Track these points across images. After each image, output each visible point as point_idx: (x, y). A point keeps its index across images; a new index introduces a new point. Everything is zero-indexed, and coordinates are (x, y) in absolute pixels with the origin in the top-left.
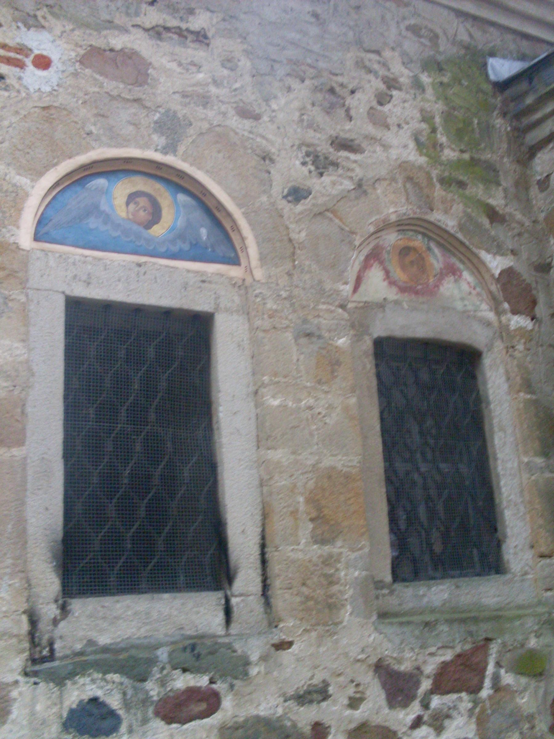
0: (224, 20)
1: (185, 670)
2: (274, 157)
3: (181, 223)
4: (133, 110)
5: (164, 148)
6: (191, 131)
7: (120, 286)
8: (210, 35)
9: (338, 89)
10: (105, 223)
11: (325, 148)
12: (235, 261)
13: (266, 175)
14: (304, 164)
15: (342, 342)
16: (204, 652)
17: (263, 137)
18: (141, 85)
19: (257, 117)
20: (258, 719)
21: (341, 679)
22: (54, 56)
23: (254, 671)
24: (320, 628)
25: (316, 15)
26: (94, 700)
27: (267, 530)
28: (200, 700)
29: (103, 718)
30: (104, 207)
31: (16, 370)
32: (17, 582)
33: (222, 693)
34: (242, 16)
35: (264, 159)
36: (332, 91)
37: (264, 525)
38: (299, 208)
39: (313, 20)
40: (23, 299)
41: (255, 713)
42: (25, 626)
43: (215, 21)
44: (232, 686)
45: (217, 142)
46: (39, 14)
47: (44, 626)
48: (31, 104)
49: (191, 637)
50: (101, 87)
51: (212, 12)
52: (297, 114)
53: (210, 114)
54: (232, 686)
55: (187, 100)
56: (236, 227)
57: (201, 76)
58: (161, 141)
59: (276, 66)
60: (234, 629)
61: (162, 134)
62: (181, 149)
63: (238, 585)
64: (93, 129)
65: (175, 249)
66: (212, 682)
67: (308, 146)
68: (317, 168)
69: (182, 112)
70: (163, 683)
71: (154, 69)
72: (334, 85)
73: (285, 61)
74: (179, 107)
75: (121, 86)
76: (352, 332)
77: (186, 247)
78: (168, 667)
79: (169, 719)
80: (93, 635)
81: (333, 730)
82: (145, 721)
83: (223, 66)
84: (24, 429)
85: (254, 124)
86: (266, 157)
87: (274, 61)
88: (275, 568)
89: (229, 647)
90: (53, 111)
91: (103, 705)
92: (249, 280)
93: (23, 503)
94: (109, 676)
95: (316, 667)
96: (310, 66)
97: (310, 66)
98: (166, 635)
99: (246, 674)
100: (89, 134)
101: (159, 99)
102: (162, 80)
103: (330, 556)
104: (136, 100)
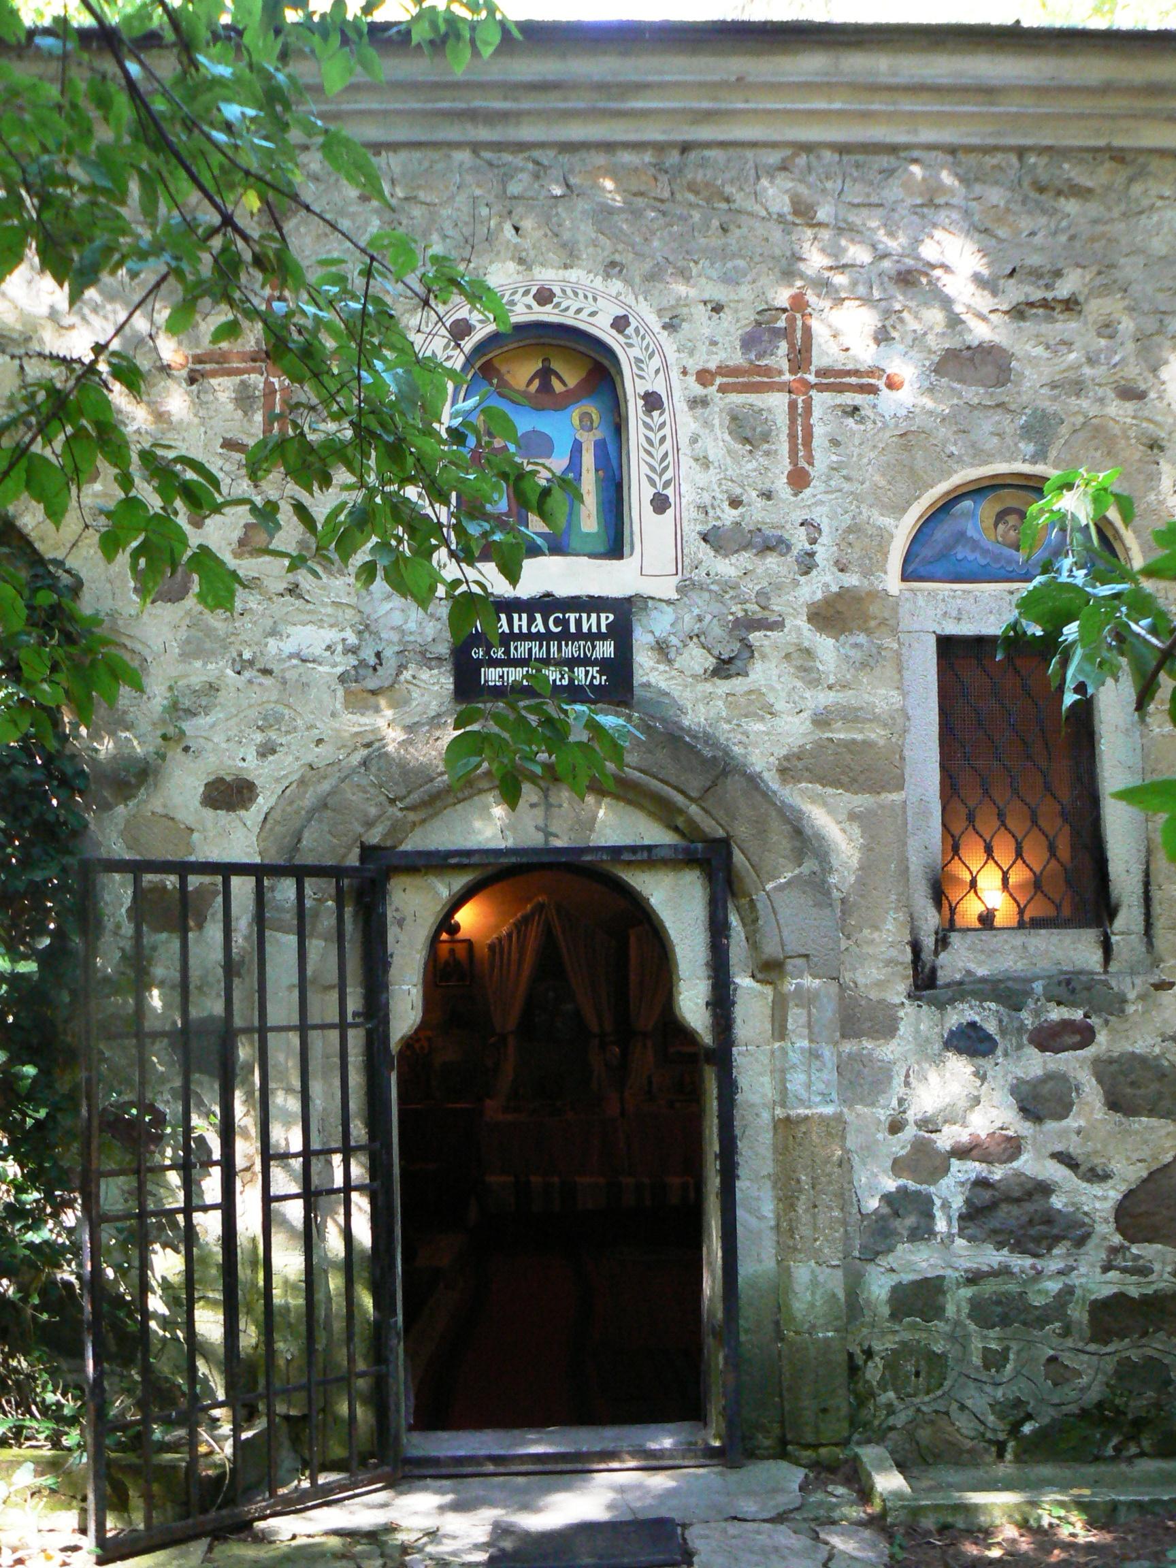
0: (1099, 273)
1: (1059, 1003)
2: (1164, 443)
5: (1033, 457)
6: (1064, 430)
7: (992, 618)
8: (1081, 299)
10: (973, 550)
16: (1078, 987)
17: (1150, 420)
19: (1141, 396)
23: (1131, 1009)
26: (973, 1025)
27: (1152, 867)
28: (1074, 1033)
29: (981, 1041)
31: (893, 718)
32: (901, 916)
33: (1097, 1028)
34: (1122, 261)
35: (1151, 447)
37: (1148, 863)
40: (896, 646)
42: (908, 956)
43: (1088, 278)
44: (1107, 1022)
45: (1094, 437)
47: (927, 956)
48: (888, 434)
49: (1066, 973)
50: (960, 397)
51: (1084, 267)
53: (1085, 404)
54: (1107, 1022)
55: (1056, 392)
57: (1073, 356)
58: (1028, 448)
60: (1113, 968)
61: (1030, 440)
62: (1053, 454)
63: (1119, 923)
64: (953, 449)
66: (1086, 1016)
70: (1037, 1013)
71: (1018, 360)
74: (1048, 403)
75: (982, 391)
78: (1043, 1000)
79: (1043, 1048)
80: (972, 966)
82: (1020, 1047)
83: (1099, 335)
84: (903, 775)
85: (1140, 404)
87: (1164, 313)
88: (1157, 909)
89: (1106, 983)
90: (911, 437)
91: (981, 1029)
93: (905, 844)
94: (986, 1004)
98: (1043, 969)
99: (1123, 1011)
100: (951, 455)
101: (1024, 398)
102: (1027, 373)
104: (999, 405)
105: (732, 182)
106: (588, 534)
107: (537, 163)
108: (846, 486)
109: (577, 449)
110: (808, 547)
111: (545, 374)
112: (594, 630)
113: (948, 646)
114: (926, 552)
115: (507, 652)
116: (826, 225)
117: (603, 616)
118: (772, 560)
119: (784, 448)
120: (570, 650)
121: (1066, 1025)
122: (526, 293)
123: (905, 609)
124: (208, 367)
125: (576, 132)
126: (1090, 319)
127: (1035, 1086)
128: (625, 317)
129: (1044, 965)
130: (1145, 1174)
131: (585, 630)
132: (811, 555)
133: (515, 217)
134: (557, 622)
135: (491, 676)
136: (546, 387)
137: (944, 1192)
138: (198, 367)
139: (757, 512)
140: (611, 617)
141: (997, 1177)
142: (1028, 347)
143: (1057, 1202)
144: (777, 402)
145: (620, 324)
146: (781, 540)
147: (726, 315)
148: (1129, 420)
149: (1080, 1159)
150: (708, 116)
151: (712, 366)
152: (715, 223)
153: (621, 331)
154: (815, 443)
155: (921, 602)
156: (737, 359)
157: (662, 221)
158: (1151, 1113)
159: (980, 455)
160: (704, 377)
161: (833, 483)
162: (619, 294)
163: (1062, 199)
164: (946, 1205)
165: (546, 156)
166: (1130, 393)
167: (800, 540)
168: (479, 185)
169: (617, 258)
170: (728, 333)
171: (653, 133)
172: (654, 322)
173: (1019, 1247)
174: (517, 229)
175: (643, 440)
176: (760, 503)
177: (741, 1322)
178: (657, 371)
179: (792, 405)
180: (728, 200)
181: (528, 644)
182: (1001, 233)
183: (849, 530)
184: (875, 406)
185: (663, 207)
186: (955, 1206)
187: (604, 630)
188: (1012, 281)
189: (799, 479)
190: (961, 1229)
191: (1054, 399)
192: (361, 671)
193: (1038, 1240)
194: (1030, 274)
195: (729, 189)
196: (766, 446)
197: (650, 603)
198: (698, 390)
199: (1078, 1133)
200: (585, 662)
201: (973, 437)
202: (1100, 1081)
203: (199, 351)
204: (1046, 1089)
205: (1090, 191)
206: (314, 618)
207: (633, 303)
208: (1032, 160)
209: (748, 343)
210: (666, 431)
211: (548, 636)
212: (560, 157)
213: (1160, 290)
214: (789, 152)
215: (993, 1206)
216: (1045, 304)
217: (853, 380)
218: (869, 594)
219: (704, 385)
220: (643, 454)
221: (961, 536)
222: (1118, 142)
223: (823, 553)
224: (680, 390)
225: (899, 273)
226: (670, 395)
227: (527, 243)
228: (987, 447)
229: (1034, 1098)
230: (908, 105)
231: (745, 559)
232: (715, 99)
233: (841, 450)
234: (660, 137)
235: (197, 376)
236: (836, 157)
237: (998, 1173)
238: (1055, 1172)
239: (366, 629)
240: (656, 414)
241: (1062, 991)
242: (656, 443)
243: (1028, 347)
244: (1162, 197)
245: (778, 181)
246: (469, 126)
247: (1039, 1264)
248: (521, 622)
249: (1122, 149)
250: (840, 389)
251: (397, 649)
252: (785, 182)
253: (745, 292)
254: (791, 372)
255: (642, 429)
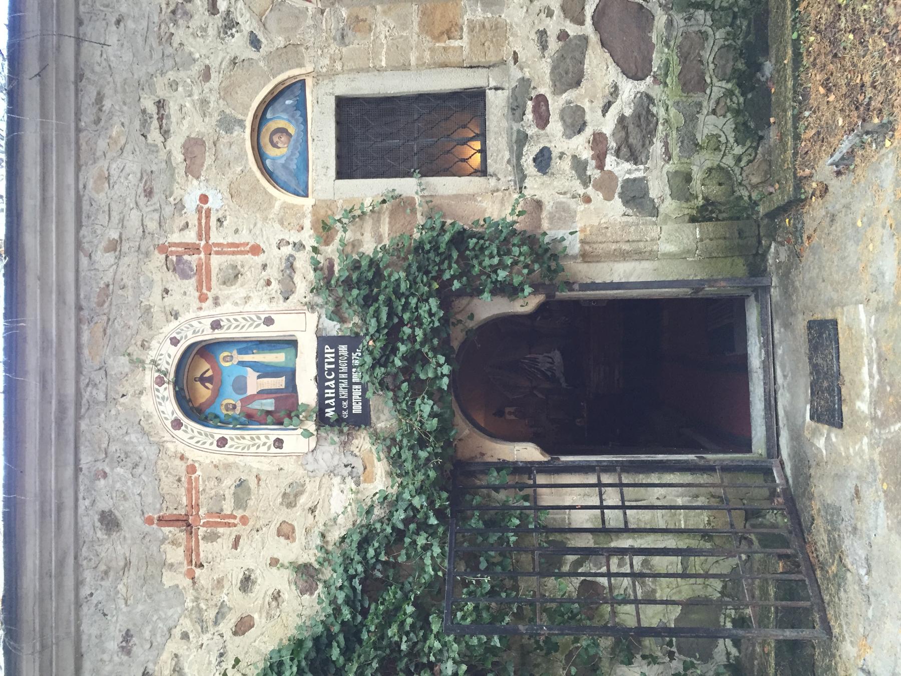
1: (524, 114)
3: (285, 116)
4: (222, 146)
6: (228, 111)
7: (327, 150)
8: (157, 99)
9: (172, 8)
10: (292, 160)
11: (218, 20)
12: (303, 82)
13: (245, 63)
14: (233, 36)
15: (344, 13)
16: (516, 104)
17: (221, 63)
18: (204, 142)
20: (552, 72)
21: (536, 22)
22: (199, 193)
23: (527, 75)
24: (508, 35)
25: (118, 22)
26: (535, 160)
29: (543, 156)
30: (283, 161)
33: (537, 93)
34: (136, 76)
35: (235, 64)
36: (174, 12)
38: (263, 40)
39: (122, 24)
41: (548, 75)
44: (534, 88)
46: (173, 203)
52: (198, 39)
55: (207, 114)
56: (282, 83)
57: (188, 105)
59: (166, 53)
62: (240, 117)
65: (301, 120)
66: (531, 99)
67: (219, 33)
68: (233, 26)
69: (216, 117)
72: (169, 10)
73: (162, 47)
75: (207, 154)
76: (337, 5)
77: (299, 113)
81: (563, 28)
86: (234, 62)
88: (475, 61)
92: (314, 74)
95: (528, 37)
96: (160, 29)
97: (160, 29)
99: (528, 79)
103: (469, 26)
105: (98, 283)
106: (286, 357)
107: (88, 385)
108: (259, 225)
109: (242, 363)
110: (291, 246)
111: (203, 380)
112: (333, 355)
113: (341, 174)
114: (293, 185)
115: (345, 400)
116: (121, 234)
117: (326, 351)
118: (298, 264)
119: (239, 257)
120: (344, 368)
121: (535, 110)
122: (158, 390)
123: (322, 196)
124: (194, 557)
125: (70, 365)
126: (168, 95)
127: (567, 126)
128: (171, 339)
129: (505, 124)
130: (614, 64)
131: (333, 360)
132: (295, 244)
133: (117, 397)
134: (330, 374)
135: (357, 409)
136: (210, 380)
137: (622, 173)
138: (194, 563)
139: (273, 273)
140: (327, 346)
141: (615, 145)
142: (184, 128)
143: (628, 112)
144: (216, 261)
145: (175, 342)
146: (288, 259)
147: (170, 287)
148: (221, 75)
149: (606, 101)
150: (61, 293)
151: (197, 294)
152: (120, 292)
153: (179, 341)
154: (237, 242)
155: (319, 187)
156: (193, 281)
157: (119, 319)
158: (582, 62)
159: (242, 155)
160: (203, 298)
161: (258, 233)
162: (159, 342)
163: (104, 108)
164: (629, 172)
165: (84, 381)
166: (206, 74)
167: (287, 250)
168: (99, 415)
169: (139, 343)
170: (180, 286)
171: (71, 324)
172: (174, 324)
173: (653, 132)
174: (123, 395)
175: (236, 330)
176: (268, 269)
177: (691, 278)
178: (200, 323)
179: (217, 253)
180: (108, 286)
181: (341, 389)
182: (123, 142)
183: (282, 224)
184: (217, 210)
185: (112, 319)
186: (630, 167)
187: (333, 350)
188: (148, 136)
189: (256, 250)
190: (642, 163)
191: (211, 115)
192: (354, 475)
193: (648, 123)
194: (144, 127)
195: (102, 285)
196: (239, 267)
197: (320, 326)
198: (210, 302)
199: (592, 102)
200: (349, 359)
201: (232, 159)
202: (565, 91)
203: (186, 563)
204: (569, 121)
205: (99, 93)
206: (327, 500)
207: (164, 335)
208: (83, 124)
209: (185, 276)
210: (231, 318)
211: (337, 379)
212: (84, 373)
213: (151, 57)
214: (81, 254)
215: (630, 147)
216: (160, 119)
217: (203, 221)
218: (314, 215)
219: (207, 299)
220: (244, 330)
221: (285, 166)
222: (72, 77)
223: (294, 237)
224: (210, 312)
225: (146, 196)
226: (212, 316)
227: (131, 392)
228: (237, 151)
229: (573, 126)
230: (53, 190)
231: (297, 278)
232: (51, 292)
233: (240, 229)
234: (73, 321)
235: (198, 563)
236: (84, 228)
237: (613, 144)
238: (613, 112)
239: (332, 472)
240: (222, 324)
241: (518, 112)
242: (237, 323)
243: (184, 128)
244: (101, 55)
245: (97, 259)
246: (66, 422)
247: (661, 121)
248: (329, 393)
249: (76, 75)
250: (208, 228)
251: (343, 456)
252: (98, 256)
253: (157, 277)
254: (199, 254)
255: (231, 330)
